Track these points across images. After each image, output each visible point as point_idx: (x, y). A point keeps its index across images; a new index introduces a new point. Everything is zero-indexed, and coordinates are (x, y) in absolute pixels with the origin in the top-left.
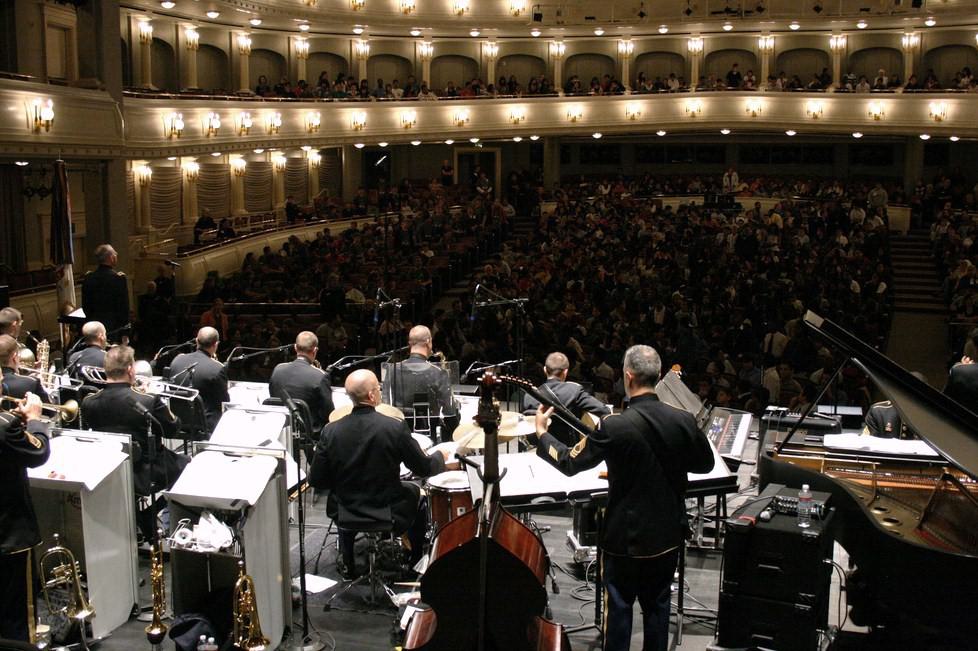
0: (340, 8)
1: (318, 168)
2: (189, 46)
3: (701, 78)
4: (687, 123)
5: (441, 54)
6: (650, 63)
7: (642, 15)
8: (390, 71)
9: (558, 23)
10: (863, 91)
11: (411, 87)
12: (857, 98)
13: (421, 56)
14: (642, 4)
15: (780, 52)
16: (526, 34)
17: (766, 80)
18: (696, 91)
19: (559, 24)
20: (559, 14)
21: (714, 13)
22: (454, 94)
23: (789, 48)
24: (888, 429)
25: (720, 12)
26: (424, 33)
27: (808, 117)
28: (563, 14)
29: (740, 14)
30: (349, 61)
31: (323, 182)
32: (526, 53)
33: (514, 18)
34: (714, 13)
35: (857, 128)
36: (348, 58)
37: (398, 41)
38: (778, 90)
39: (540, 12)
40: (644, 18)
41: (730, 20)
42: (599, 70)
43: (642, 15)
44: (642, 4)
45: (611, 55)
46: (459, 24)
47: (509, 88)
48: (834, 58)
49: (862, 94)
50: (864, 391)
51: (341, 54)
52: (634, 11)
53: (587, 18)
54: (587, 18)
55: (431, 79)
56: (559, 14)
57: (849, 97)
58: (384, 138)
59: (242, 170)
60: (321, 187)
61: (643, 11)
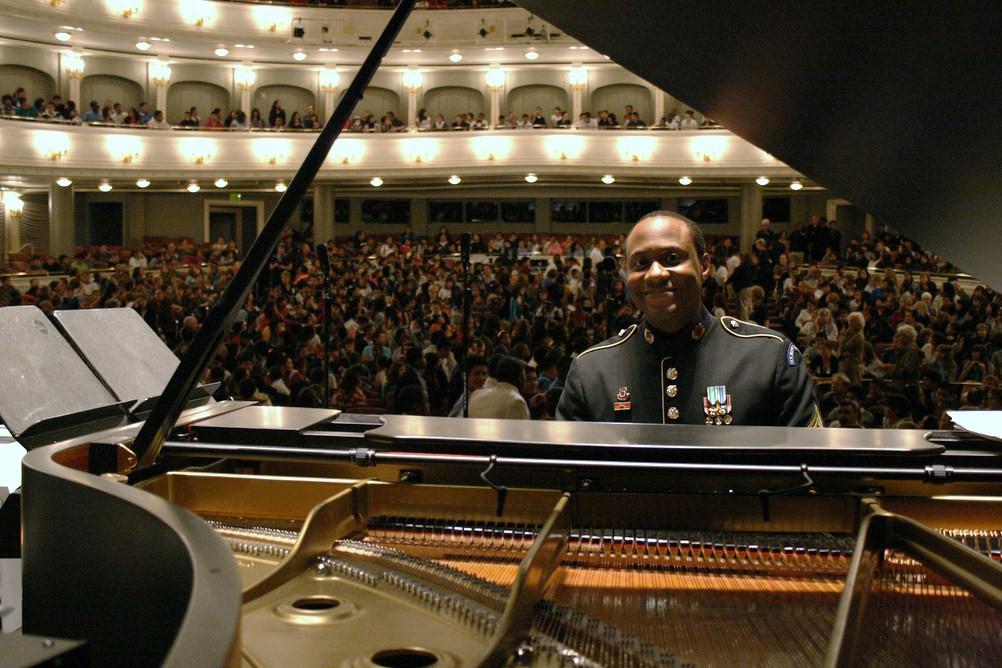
0: (100, 11)
1: (18, 216)
2: (71, 76)
3: (502, 118)
4: (335, 171)
5: (182, 79)
6: (444, 99)
7: (427, 35)
8: (107, 94)
9: (325, 42)
10: (688, 128)
11: (139, 113)
12: (682, 135)
13: (68, 71)
14: (428, 22)
15: (595, 87)
16: (206, 53)
17: (578, 118)
18: (496, 129)
19: (328, 44)
20: (326, 29)
21: (514, 36)
22: (189, 122)
23: (605, 84)
24: (828, 372)
25: (522, 36)
26: (156, 50)
27: (698, 160)
28: (330, 31)
29: (544, 37)
30: (145, 90)
31: (25, 236)
32: (28, 64)
33: (269, 34)
34: (514, 36)
35: (608, 169)
36: (55, 76)
37: (124, 60)
38: (593, 128)
39: (300, 27)
40: (431, 40)
41: (534, 44)
42: (464, 104)
43: (427, 35)
44: (428, 22)
45: (394, 89)
46: (126, 30)
47: (100, 115)
48: (575, 95)
49: (687, 132)
50: (485, 475)
51: (45, 69)
52: (419, 31)
53: (361, 38)
54: (361, 38)
55: (167, 108)
56: (326, 29)
57: (674, 135)
58: (532, 168)
59: (18, 213)
60: (23, 240)
61: (429, 29)
